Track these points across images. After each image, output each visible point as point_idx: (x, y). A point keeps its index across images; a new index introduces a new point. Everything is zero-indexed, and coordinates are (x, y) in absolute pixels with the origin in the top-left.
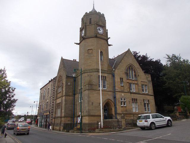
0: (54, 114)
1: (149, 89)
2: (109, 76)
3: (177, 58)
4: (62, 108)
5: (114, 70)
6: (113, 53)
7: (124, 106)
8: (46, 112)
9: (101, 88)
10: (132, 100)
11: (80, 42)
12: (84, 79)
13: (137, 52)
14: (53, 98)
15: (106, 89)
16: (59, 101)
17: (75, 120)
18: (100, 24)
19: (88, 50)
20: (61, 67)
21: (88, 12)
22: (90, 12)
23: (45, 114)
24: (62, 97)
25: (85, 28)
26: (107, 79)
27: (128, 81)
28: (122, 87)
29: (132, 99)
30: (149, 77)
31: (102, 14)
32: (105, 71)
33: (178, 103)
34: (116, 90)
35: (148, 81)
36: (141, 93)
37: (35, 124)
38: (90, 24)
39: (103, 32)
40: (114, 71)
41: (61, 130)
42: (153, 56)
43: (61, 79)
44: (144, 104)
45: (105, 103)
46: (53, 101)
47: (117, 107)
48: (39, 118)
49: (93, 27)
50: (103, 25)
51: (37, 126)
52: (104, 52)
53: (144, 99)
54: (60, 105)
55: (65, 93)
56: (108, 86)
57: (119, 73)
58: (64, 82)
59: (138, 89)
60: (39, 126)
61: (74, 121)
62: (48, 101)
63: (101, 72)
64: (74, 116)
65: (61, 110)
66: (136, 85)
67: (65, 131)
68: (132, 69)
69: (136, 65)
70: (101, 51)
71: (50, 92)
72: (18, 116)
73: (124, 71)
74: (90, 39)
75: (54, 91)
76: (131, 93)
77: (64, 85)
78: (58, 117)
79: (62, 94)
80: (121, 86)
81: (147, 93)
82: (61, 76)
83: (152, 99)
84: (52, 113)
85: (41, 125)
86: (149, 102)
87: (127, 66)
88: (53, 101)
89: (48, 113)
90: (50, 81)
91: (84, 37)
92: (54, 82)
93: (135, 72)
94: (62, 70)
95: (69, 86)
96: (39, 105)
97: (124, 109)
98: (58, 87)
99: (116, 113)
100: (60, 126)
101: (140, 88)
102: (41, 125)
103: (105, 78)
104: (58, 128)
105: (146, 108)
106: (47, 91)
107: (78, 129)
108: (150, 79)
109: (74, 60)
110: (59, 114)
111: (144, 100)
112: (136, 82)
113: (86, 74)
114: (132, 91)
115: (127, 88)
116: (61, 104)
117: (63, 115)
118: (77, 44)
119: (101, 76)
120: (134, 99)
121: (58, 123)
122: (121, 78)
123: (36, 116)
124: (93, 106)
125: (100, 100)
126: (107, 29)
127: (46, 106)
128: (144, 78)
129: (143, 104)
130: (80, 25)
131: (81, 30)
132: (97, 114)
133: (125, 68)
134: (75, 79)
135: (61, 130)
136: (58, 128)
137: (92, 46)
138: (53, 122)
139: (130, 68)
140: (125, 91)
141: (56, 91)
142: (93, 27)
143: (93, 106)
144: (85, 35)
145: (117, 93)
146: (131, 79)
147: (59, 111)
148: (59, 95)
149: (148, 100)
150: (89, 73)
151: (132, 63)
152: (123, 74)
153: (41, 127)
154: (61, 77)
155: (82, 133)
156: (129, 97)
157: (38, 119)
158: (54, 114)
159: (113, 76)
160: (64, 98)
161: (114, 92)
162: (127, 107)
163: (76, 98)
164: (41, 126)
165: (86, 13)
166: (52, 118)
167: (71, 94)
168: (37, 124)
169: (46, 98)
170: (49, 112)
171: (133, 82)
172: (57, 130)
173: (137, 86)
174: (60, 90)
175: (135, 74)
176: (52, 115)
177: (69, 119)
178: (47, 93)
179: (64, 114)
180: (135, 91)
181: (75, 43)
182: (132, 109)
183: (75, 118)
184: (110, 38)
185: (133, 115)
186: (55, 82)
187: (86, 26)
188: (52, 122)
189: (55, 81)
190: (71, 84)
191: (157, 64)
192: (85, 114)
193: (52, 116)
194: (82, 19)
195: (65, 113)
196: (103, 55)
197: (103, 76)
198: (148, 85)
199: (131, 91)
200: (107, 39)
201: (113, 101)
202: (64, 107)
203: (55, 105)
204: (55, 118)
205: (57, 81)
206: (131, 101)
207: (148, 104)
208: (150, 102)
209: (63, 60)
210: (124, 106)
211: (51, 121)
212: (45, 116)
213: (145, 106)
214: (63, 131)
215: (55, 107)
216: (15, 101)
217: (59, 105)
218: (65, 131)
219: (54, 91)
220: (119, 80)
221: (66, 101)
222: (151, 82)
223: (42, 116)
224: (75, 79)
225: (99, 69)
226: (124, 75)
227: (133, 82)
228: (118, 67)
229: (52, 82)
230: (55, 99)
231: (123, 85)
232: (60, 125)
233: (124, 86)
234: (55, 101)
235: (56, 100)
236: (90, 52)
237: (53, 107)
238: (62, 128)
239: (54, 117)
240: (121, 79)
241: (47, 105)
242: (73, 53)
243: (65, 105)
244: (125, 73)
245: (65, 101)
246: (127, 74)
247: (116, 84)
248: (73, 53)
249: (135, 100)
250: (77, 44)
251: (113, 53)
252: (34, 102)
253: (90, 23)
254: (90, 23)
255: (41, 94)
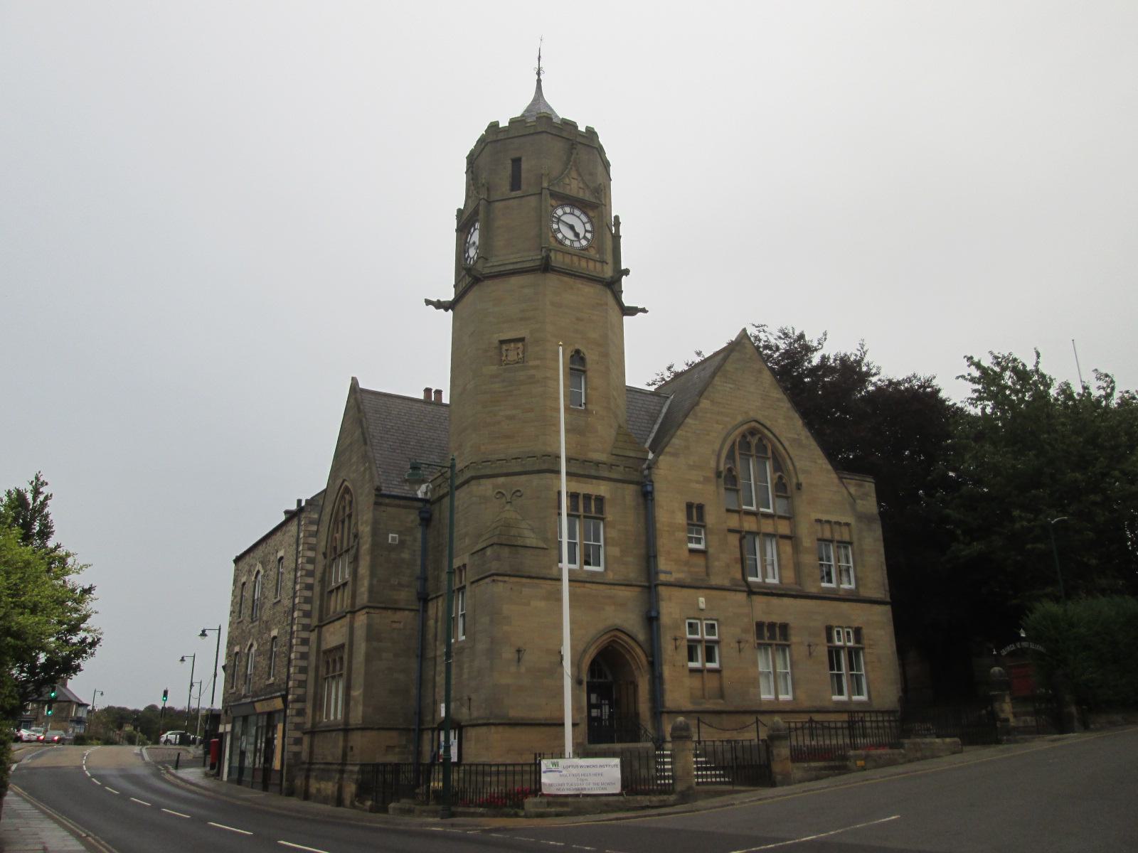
0: (309, 711)
1: (864, 567)
2: (619, 501)
3: (1022, 375)
4: (354, 676)
5: (651, 456)
6: (651, 353)
7: (709, 665)
8: (268, 692)
9: (565, 566)
10: (759, 634)
11: (460, 296)
12: (476, 509)
13: (812, 338)
14: (307, 614)
15: (600, 569)
16: (334, 636)
17: (427, 748)
18: (573, 187)
19: (502, 342)
20: (348, 442)
21: (504, 123)
22: (513, 122)
23: (260, 707)
24: (353, 612)
25: (481, 215)
26: (610, 514)
27: (733, 521)
28: (700, 561)
29: (760, 626)
30: (864, 496)
31: (582, 128)
32: (597, 464)
33: (1011, 648)
34: (663, 577)
35: (861, 517)
36: (813, 590)
37: (209, 761)
38: (514, 194)
39: (589, 236)
40: (649, 468)
41: (347, 802)
42: (890, 364)
43: (347, 511)
44: (830, 653)
45: (592, 652)
46: (304, 635)
47: (667, 672)
48: (229, 728)
49: (535, 200)
50: (588, 196)
51: (218, 774)
52: (591, 356)
53: (834, 623)
54: (341, 659)
55: (371, 590)
56: (615, 551)
57: (681, 476)
58: (365, 530)
59: (798, 567)
60: (225, 777)
61: (419, 753)
62: (274, 633)
63: (568, 474)
64: (421, 721)
65: (348, 689)
66: (788, 542)
67: (369, 803)
68: (762, 448)
69: (787, 426)
70: (578, 352)
71: (290, 584)
72: (109, 710)
73: (713, 464)
74: (515, 281)
75: (310, 574)
76: (751, 591)
77: (365, 547)
78: (330, 729)
79: (354, 596)
80: (692, 551)
81: (853, 586)
82: (347, 490)
83: (878, 626)
84: (298, 705)
85: (241, 769)
86: (858, 640)
87: (729, 434)
88: (304, 635)
89: (278, 704)
90: (291, 516)
91: (479, 266)
92: (312, 522)
93: (778, 467)
94: (354, 459)
95: (391, 548)
96: (229, 655)
97: (712, 683)
98: (334, 553)
99: (658, 710)
100: (341, 779)
101: (809, 559)
102: (241, 769)
103: (600, 509)
104: (329, 787)
105: (839, 677)
106: (272, 574)
107: (439, 796)
108: (870, 505)
109: (428, 391)
110: (334, 712)
111: (829, 630)
112: (784, 528)
113: (486, 487)
114: (759, 580)
115: (728, 566)
116: (346, 657)
117: (357, 716)
118: (439, 305)
119: (573, 497)
120: (772, 626)
121: (330, 759)
122: (689, 506)
123: (213, 717)
124: (523, 669)
125: (572, 622)
126: (613, 215)
127: (263, 663)
128: (834, 500)
129: (822, 652)
130: (455, 194)
131: (465, 223)
132: (540, 715)
133: (717, 446)
134: (427, 513)
135: (347, 802)
136: (329, 787)
137: (521, 319)
138: (305, 756)
139: (749, 443)
140: (715, 580)
141: (318, 574)
142: (535, 200)
143: (523, 669)
144: (483, 257)
145: (663, 591)
146: (754, 508)
147: (335, 693)
148: (338, 603)
149: (858, 632)
150: (501, 480)
151: (760, 418)
152: (707, 480)
153: (239, 782)
154: (347, 497)
155: (453, 815)
156: (738, 614)
157: (222, 737)
158: (309, 711)
159: (647, 496)
160: (361, 619)
161: (650, 587)
162: (725, 673)
163: (431, 623)
164: (239, 775)
165: (493, 127)
166: (298, 734)
167: (405, 596)
168: (216, 766)
169: (266, 614)
170: (284, 698)
171: (768, 526)
172: (325, 800)
173: (787, 547)
174: (342, 573)
175: (780, 478)
176: (301, 713)
177: (391, 738)
178: (271, 585)
179: (360, 708)
180: (776, 581)
181: (428, 302)
182: (755, 683)
183: (427, 737)
184: (627, 272)
185: (753, 718)
186: (318, 522)
187: (489, 202)
188: (297, 755)
189: (316, 516)
190: (402, 542)
191: (916, 406)
192: (475, 714)
193: (298, 720)
194: (472, 160)
195: (365, 705)
196: (589, 374)
197: (587, 497)
198: (856, 544)
199: (751, 579)
200: (613, 284)
201: (641, 637)
202: (362, 671)
203: (313, 658)
204: (312, 733)
205: (326, 518)
206: (751, 638)
207: (853, 654)
208: (865, 642)
209: (355, 390)
210: (709, 665)
211: (296, 749)
212: (263, 722)
213: (834, 662)
214: (353, 806)
215: (317, 668)
216: (85, 648)
217: (334, 660)
218: (369, 803)
219: (310, 574)
220: (681, 518)
221: (373, 635)
222: (878, 532)
223: (245, 719)
224: (427, 513)
225: (559, 457)
226: (711, 488)
227: (768, 526)
228: (675, 441)
229: (299, 525)
230: (315, 622)
231: (701, 546)
232: (342, 772)
233: (711, 551)
234: (313, 636)
235: (320, 627)
236: (512, 356)
237: (303, 670)
238: (350, 789)
239: (308, 726)
240: (695, 513)
241: (271, 656)
242: (419, 361)
243: (369, 659)
244: (718, 474)
245: (369, 638)
246: (729, 480)
247: (664, 542)
248: (419, 361)
249: (773, 635)
250: (439, 305)
251: (651, 353)
252: (182, 660)
253: (516, 183)
254: (516, 183)
255: (240, 587)
